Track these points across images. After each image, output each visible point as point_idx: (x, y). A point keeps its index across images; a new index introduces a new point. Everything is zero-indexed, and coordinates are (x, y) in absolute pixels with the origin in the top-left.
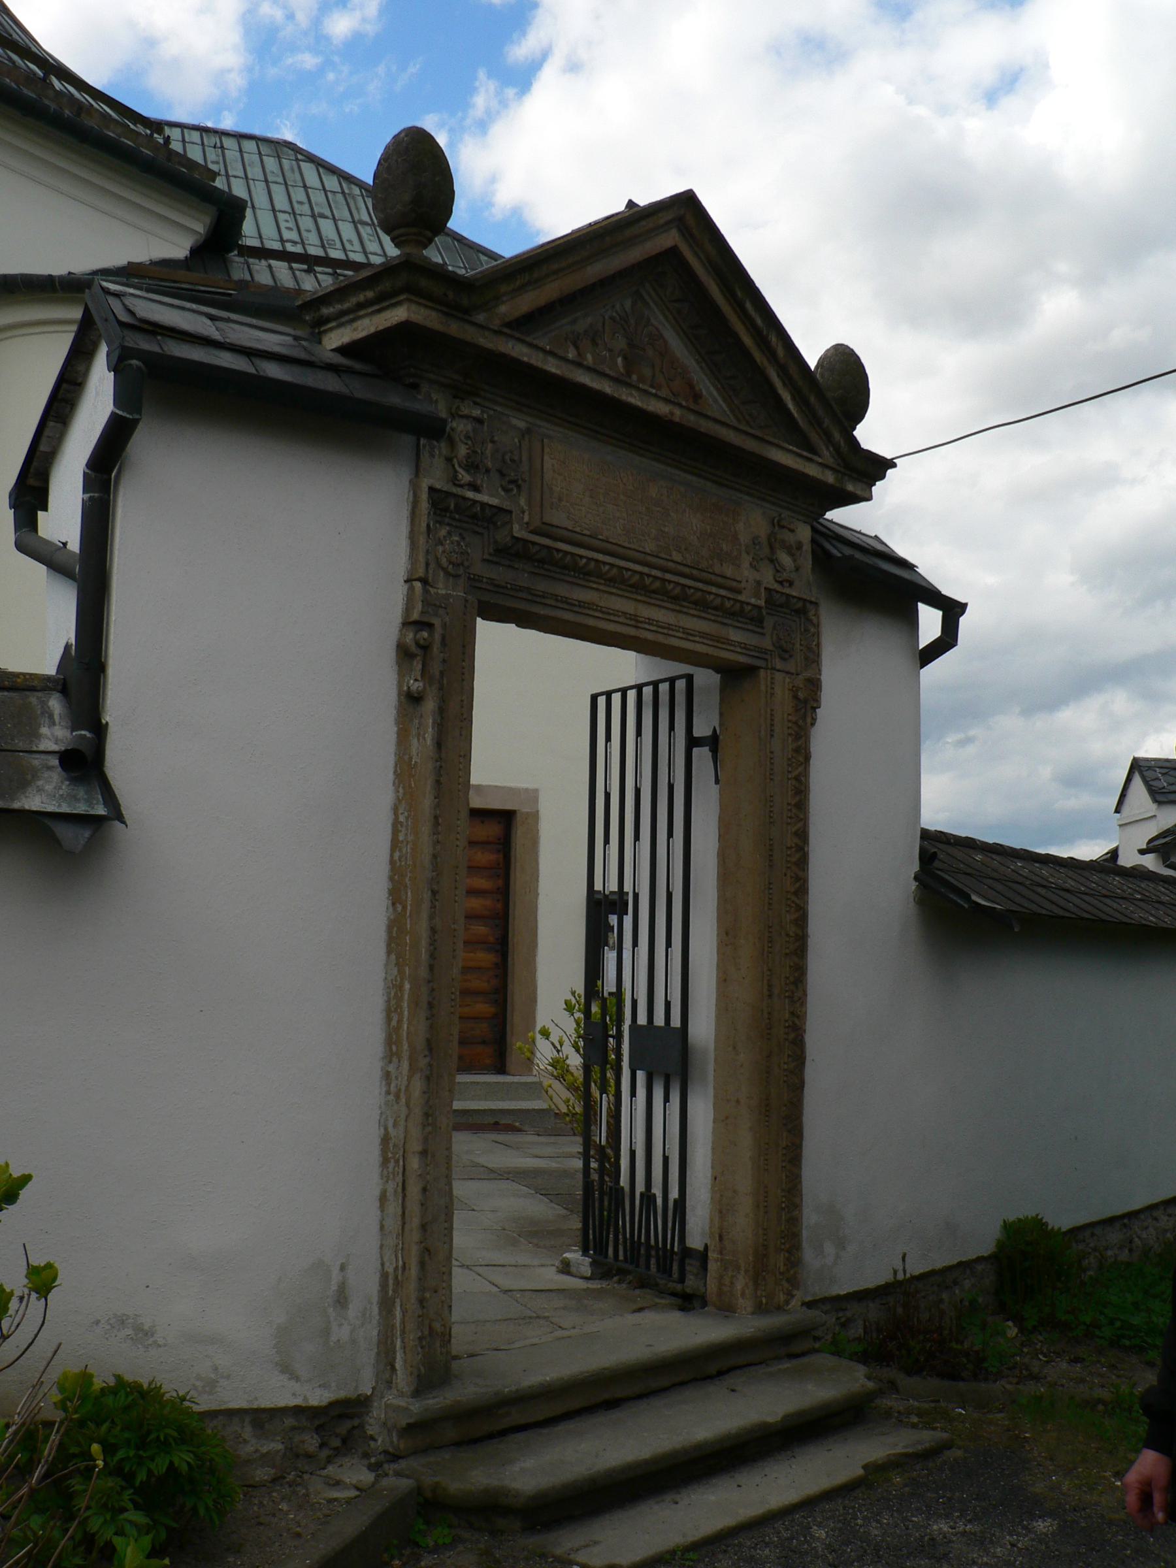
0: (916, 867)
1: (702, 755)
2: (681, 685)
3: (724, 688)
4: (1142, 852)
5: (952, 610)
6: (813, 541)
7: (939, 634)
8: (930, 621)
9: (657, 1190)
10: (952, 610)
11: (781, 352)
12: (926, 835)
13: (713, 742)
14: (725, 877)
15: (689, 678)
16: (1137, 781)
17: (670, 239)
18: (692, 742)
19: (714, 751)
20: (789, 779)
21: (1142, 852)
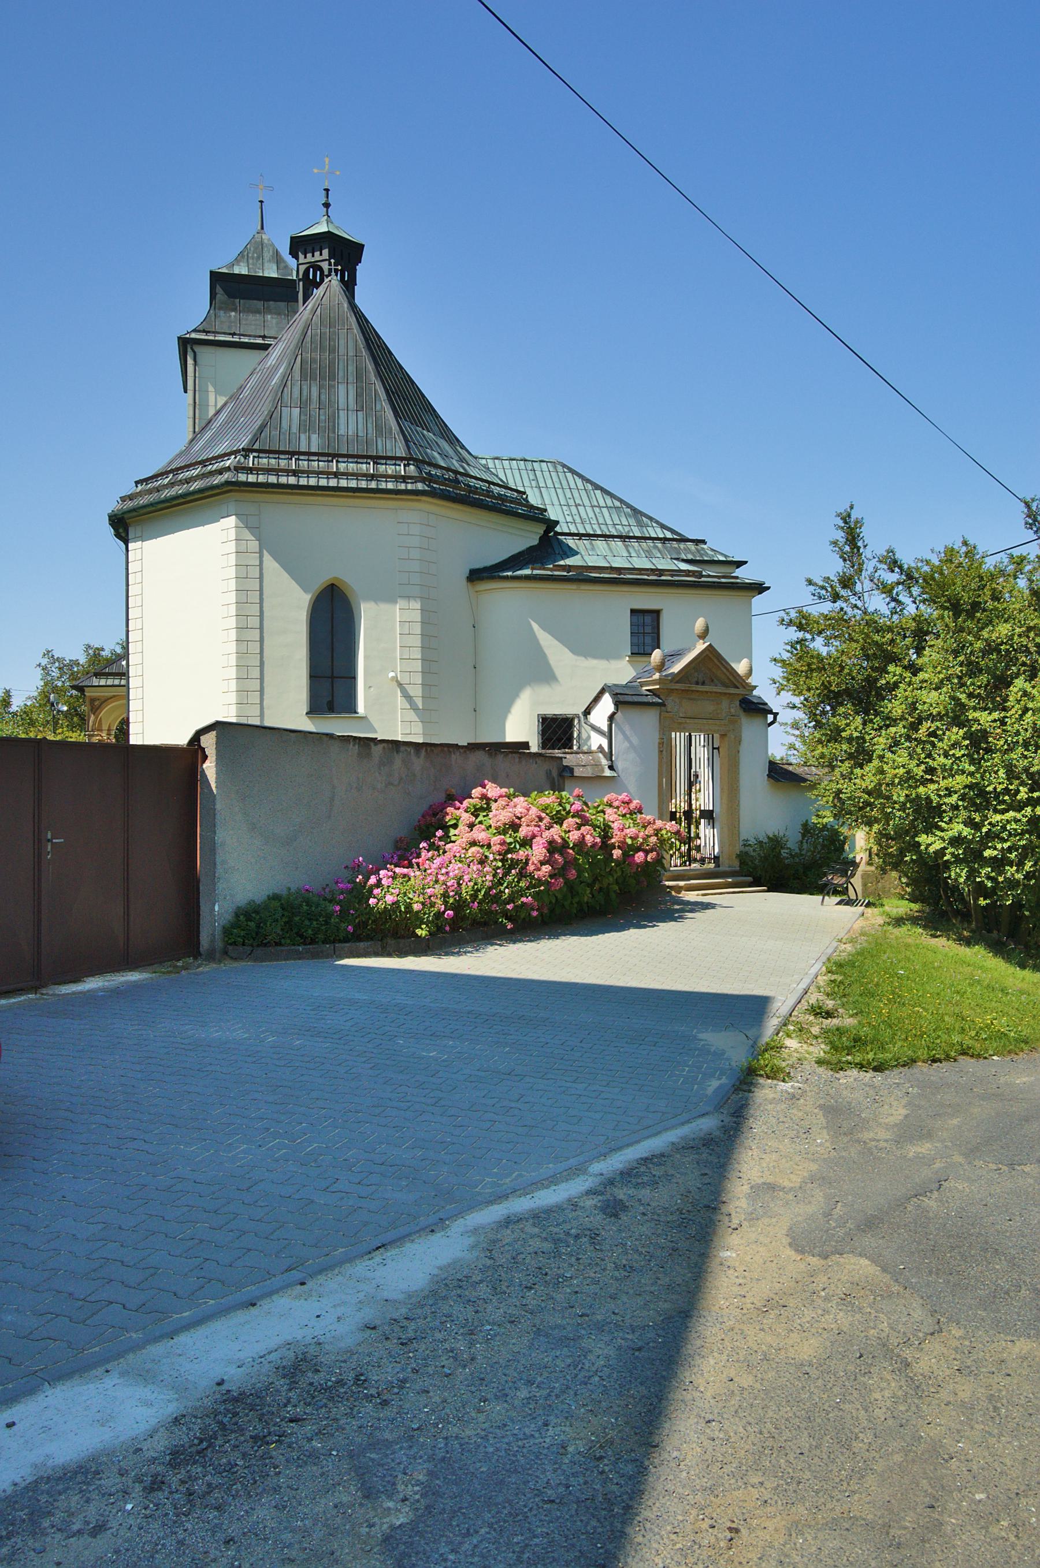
5: (776, 715)
8: (770, 718)
10: (776, 715)
13: (718, 749)
18: (713, 748)
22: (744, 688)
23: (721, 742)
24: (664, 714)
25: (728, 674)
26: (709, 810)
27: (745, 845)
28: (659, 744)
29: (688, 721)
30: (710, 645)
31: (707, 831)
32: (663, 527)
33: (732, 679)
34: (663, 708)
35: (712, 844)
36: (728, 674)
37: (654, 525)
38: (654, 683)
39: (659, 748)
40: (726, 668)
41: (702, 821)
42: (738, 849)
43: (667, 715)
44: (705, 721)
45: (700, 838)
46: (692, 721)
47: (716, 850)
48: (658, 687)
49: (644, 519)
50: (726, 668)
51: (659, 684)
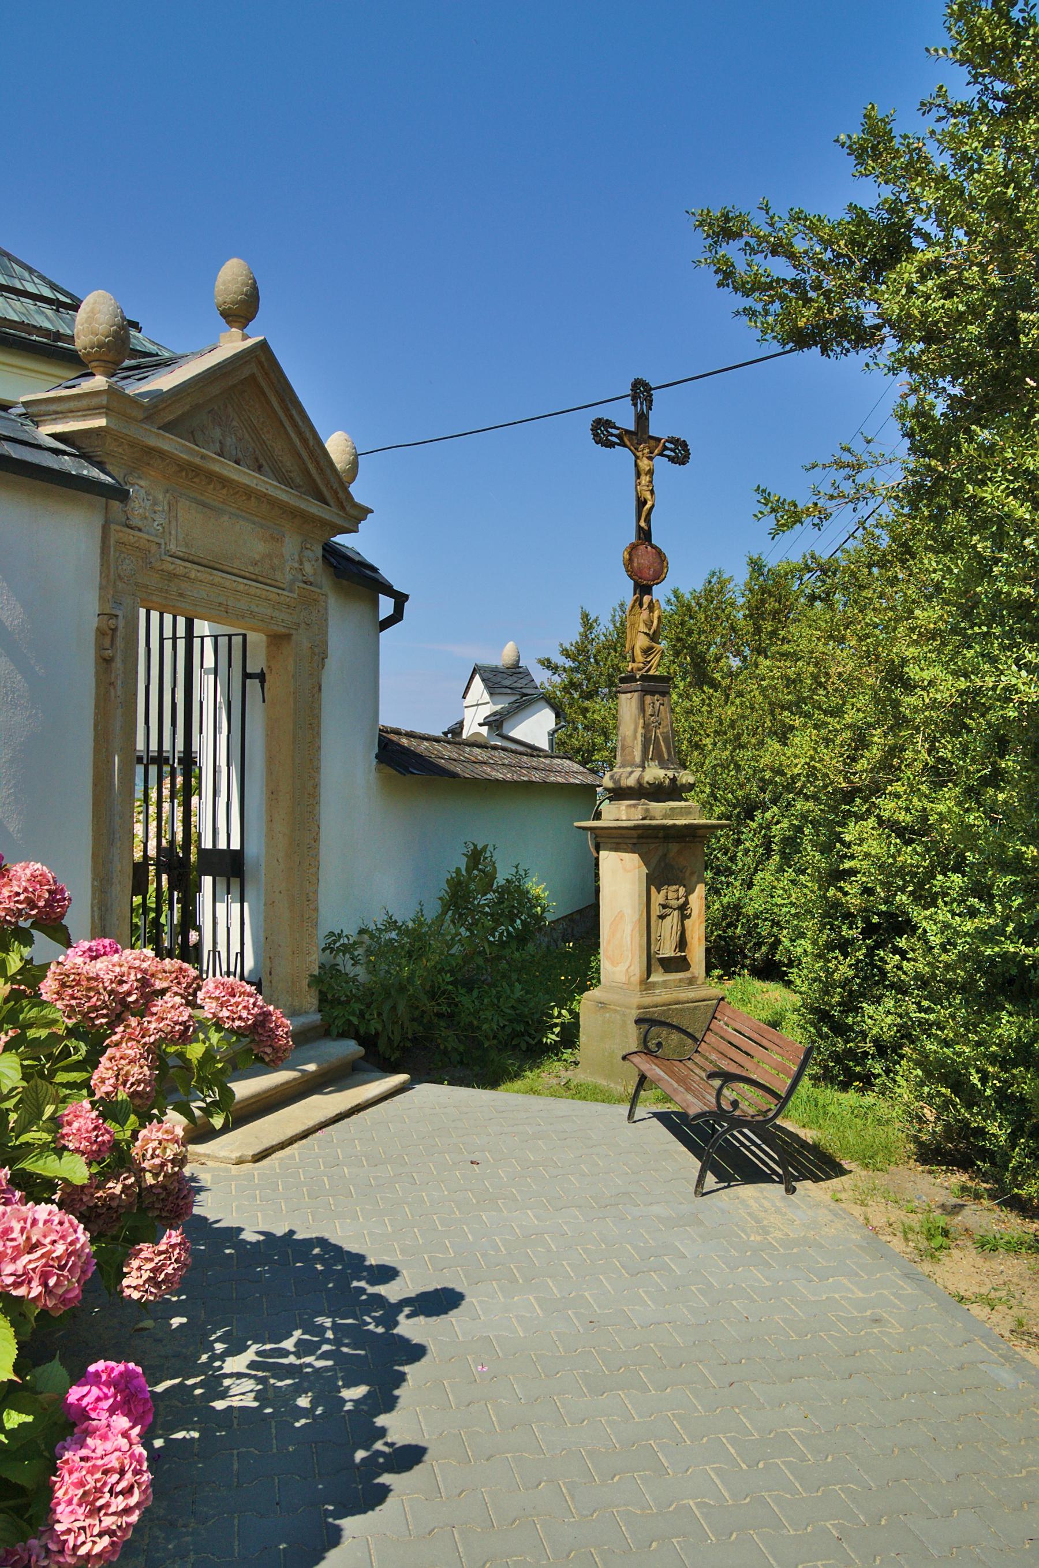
0: (376, 750)
1: (253, 685)
2: (237, 641)
3: (269, 645)
4: (480, 725)
5: (401, 599)
6: (323, 556)
7: (636, 856)
8: (386, 606)
9: (222, 948)
10: (401, 599)
11: (311, 442)
12: (384, 730)
13: (261, 677)
14: (271, 760)
15: (244, 636)
16: (477, 678)
17: (252, 369)
18: (246, 676)
19: (263, 682)
20: (744, 865)
21: (480, 725)
22: (343, 508)
23: (270, 657)
24: (117, 533)
25: (304, 454)
26: (229, 851)
27: (328, 948)
28: (100, 633)
29: (194, 571)
30: (263, 345)
31: (221, 907)
32: (53, 287)
33: (313, 471)
34: (116, 504)
35: (235, 948)
36: (304, 454)
37: (36, 280)
38: (87, 405)
39: (100, 648)
40: (300, 434)
41: (207, 881)
42: (314, 960)
43: (130, 536)
44: (241, 584)
45: (199, 929)
46: (204, 575)
47: (249, 963)
48: (101, 422)
49: (14, 265)
50: (300, 434)
51: (106, 410)
